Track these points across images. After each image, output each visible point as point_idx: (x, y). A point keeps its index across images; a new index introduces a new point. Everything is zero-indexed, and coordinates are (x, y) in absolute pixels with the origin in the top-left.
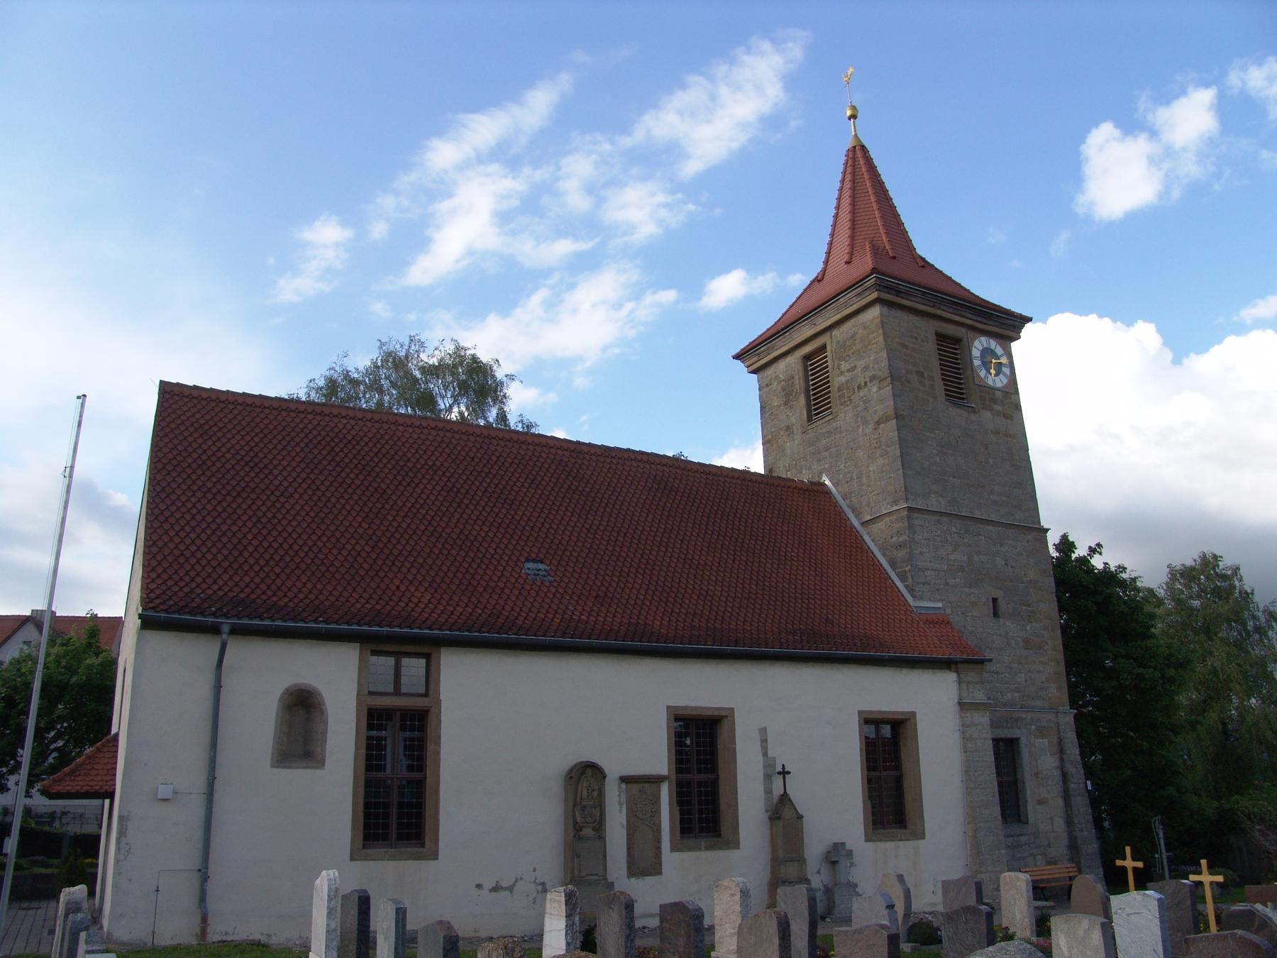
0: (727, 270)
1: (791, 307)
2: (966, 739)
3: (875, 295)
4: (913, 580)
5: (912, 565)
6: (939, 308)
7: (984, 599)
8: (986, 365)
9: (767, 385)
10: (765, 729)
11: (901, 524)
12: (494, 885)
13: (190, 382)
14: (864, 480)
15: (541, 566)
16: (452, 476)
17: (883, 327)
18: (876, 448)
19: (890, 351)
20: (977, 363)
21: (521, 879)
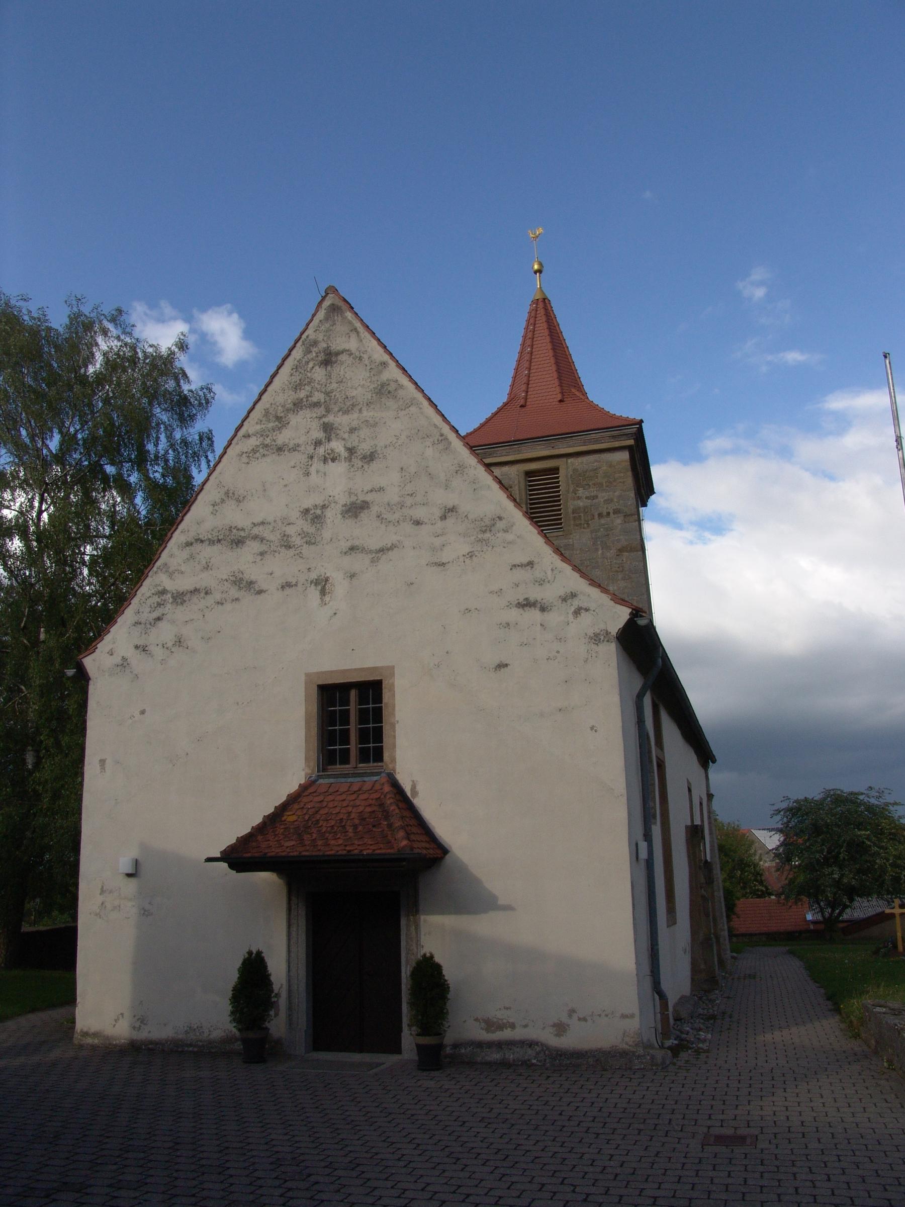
13: (712, 749)
18: (617, 571)
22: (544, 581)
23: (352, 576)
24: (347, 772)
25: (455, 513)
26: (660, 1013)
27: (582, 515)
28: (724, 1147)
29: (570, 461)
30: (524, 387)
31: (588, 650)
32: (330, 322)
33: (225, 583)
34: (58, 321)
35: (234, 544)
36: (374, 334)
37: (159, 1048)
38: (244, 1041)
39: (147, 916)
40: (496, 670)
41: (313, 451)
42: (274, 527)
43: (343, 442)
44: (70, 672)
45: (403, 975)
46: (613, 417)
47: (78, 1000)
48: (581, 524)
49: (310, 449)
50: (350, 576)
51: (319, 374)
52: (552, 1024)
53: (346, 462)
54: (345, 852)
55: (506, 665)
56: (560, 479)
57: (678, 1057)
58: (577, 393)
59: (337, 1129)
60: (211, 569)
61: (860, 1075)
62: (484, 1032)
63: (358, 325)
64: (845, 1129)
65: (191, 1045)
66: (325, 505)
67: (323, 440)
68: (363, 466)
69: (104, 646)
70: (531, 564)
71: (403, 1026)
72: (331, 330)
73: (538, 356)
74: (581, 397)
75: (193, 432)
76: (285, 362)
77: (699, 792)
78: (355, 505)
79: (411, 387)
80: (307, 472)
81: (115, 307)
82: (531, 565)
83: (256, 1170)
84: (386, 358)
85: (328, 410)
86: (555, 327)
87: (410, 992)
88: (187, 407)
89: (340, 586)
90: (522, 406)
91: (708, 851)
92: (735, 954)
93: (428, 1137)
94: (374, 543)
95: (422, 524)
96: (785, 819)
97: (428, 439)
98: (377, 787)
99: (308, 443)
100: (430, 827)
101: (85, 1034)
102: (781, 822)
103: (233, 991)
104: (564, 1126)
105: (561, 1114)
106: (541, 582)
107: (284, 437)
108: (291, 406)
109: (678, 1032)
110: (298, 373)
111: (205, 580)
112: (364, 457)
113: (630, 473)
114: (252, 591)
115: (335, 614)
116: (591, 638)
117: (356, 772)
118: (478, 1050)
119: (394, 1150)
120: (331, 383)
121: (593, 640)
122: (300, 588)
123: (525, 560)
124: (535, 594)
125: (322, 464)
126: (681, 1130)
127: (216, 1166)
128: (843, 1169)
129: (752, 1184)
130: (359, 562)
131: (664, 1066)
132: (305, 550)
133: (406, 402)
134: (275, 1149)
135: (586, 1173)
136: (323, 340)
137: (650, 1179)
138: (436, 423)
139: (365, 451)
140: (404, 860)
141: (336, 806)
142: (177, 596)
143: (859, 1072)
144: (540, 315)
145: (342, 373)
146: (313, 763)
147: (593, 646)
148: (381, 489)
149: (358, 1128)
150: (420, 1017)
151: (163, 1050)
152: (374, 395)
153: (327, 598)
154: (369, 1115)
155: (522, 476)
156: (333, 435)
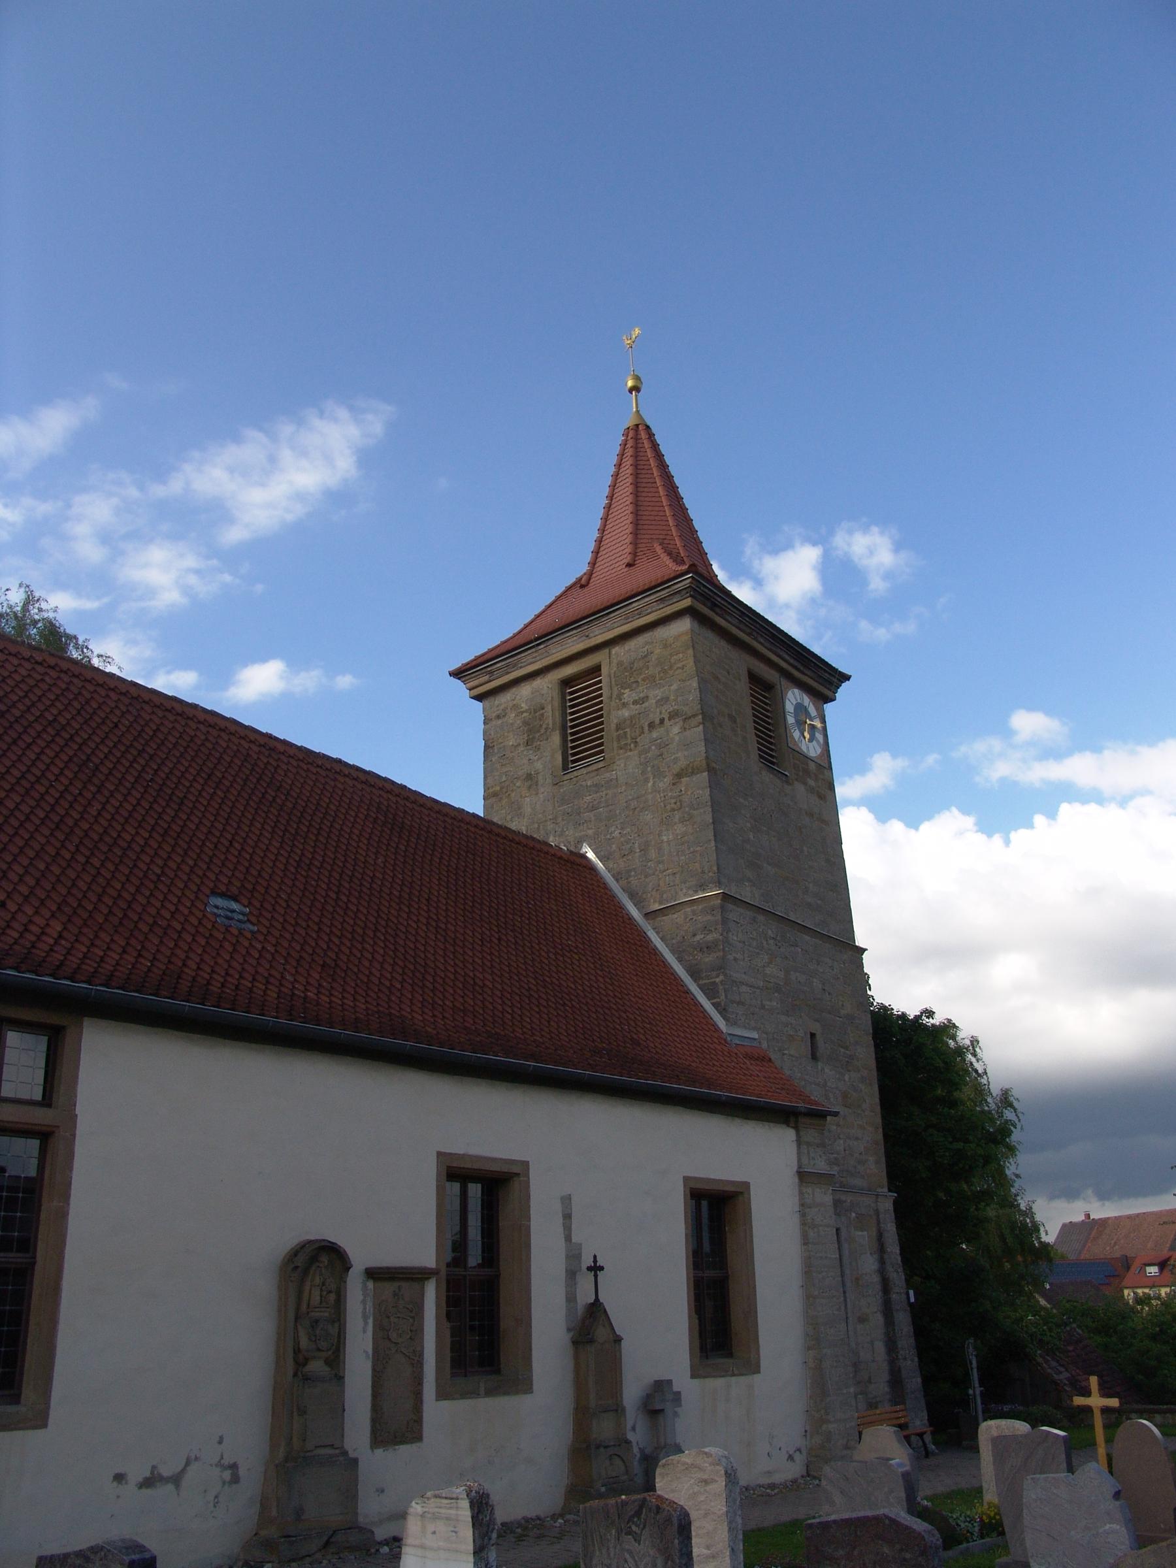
0: (263, 658)
1: (538, 616)
2: (806, 1224)
3: (687, 602)
4: (726, 997)
5: (726, 975)
6: (755, 639)
7: (802, 1033)
8: (800, 724)
9: (498, 717)
10: (569, 1197)
11: (709, 917)
12: (148, 1474)
14: (653, 854)
15: (235, 906)
16: (84, 743)
17: (694, 647)
18: (673, 810)
19: (702, 682)
20: (791, 720)
21: (196, 1459)
27: (628, 730)
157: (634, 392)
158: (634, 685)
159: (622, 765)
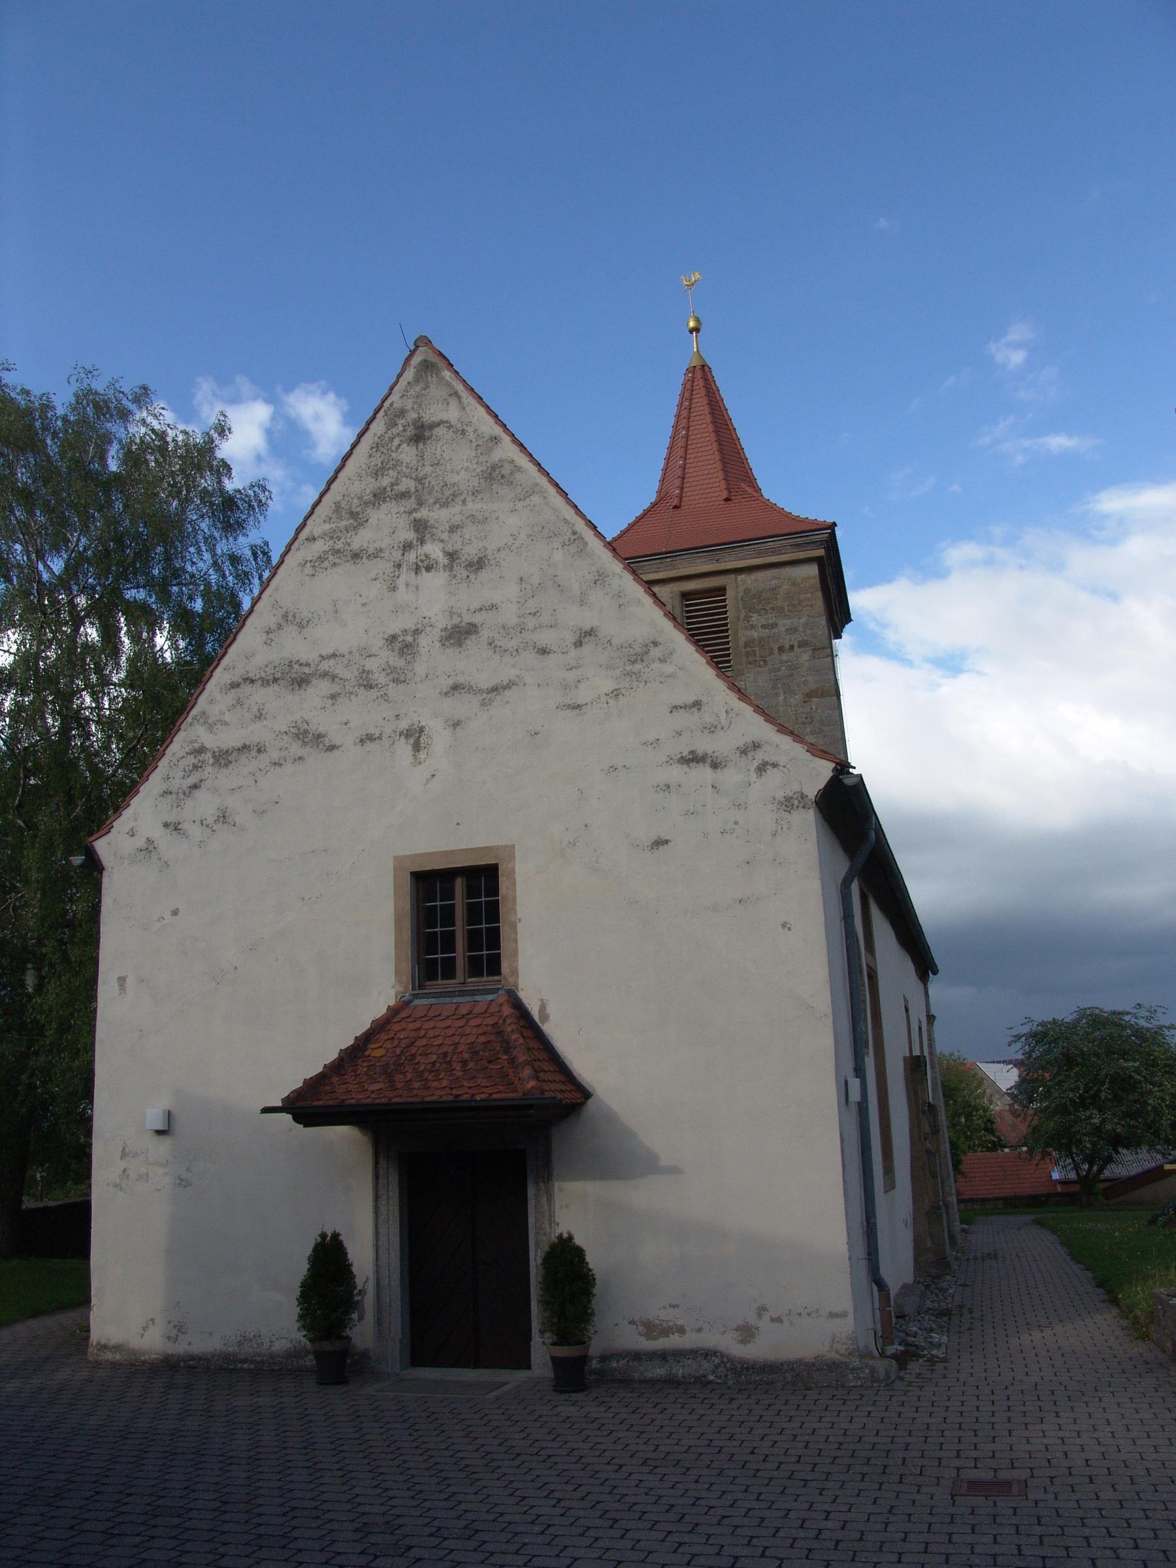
22: (716, 727)
23: (456, 724)
24: (452, 990)
25: (593, 637)
26: (879, 1309)
28: (982, 1498)
29: (740, 578)
30: (678, 482)
31: (777, 820)
32: (422, 385)
33: (284, 736)
34: (62, 402)
35: (296, 685)
36: (481, 399)
37: (203, 1364)
38: (318, 1355)
39: (185, 1187)
40: (652, 848)
41: (400, 558)
42: (350, 661)
43: (441, 545)
44: (77, 860)
45: (532, 1263)
46: (796, 519)
47: (94, 1301)
48: (756, 661)
49: (397, 555)
50: (453, 725)
51: (408, 454)
52: (736, 1326)
53: (445, 571)
54: (451, 1098)
55: (667, 842)
56: (727, 602)
57: (906, 1369)
58: (748, 489)
59: (446, 1478)
60: (266, 719)
61: (1157, 1391)
62: (643, 1339)
63: (460, 387)
64: (1147, 1469)
65: (245, 1361)
66: (417, 630)
67: (415, 543)
68: (468, 577)
69: (122, 824)
70: (697, 704)
71: (533, 1332)
72: (423, 395)
73: (695, 442)
74: (756, 495)
75: (243, 544)
76: (362, 439)
77: (918, 1014)
78: (458, 630)
79: (532, 469)
80: (393, 585)
81: (141, 383)
82: (698, 707)
83: (335, 1541)
84: (498, 430)
85: (420, 503)
86: (718, 402)
87: (540, 1286)
88: (232, 510)
89: (439, 738)
90: (676, 507)
91: (932, 1094)
92: (966, 1227)
93: (573, 1489)
94: (485, 680)
95: (549, 653)
96: (1027, 1047)
97: (556, 539)
98: (493, 1009)
99: (393, 547)
100: (566, 1061)
101: (104, 1347)
102: (1022, 1051)
103: (301, 1287)
104: (758, 1470)
105: (752, 1453)
106: (712, 729)
107: (362, 539)
108: (370, 497)
109: (902, 1335)
110: (379, 454)
111: (256, 733)
112: (470, 565)
113: (819, 594)
114: (321, 746)
115: (433, 776)
116: (781, 803)
117: (464, 989)
118: (635, 1363)
119: (526, 1508)
120: (424, 465)
121: (784, 806)
122: (386, 742)
123: (690, 699)
124: (704, 744)
125: (413, 573)
126: (921, 1474)
127: (279, 1535)
128: (1154, 1530)
129: (1030, 1553)
130: (463, 706)
131: (888, 1382)
132: (393, 690)
133: (525, 490)
134: (361, 1509)
135: (795, 1540)
136: (413, 408)
137: (886, 1547)
138: (568, 518)
139: (472, 556)
140: (531, 1107)
141: (439, 1035)
142: (220, 756)
143: (1155, 1388)
144: (697, 387)
145: (439, 452)
146: (406, 978)
147: (785, 815)
148: (493, 607)
149: (475, 1476)
150: (555, 1320)
151: (208, 1368)
152: (482, 481)
153: (422, 755)
154: (489, 1457)
155: (678, 598)
156: (428, 536)
157: (694, 333)
158: (763, 612)
159: (752, 678)
